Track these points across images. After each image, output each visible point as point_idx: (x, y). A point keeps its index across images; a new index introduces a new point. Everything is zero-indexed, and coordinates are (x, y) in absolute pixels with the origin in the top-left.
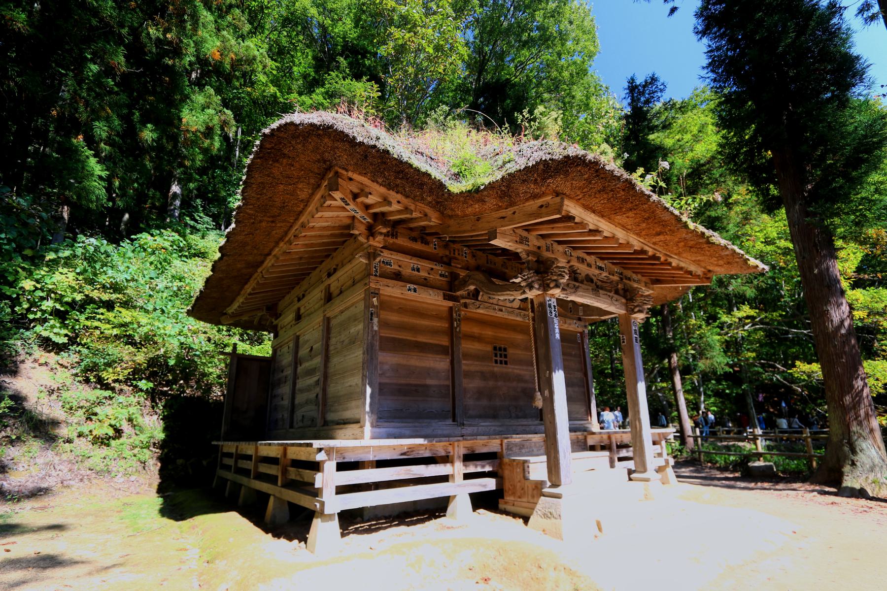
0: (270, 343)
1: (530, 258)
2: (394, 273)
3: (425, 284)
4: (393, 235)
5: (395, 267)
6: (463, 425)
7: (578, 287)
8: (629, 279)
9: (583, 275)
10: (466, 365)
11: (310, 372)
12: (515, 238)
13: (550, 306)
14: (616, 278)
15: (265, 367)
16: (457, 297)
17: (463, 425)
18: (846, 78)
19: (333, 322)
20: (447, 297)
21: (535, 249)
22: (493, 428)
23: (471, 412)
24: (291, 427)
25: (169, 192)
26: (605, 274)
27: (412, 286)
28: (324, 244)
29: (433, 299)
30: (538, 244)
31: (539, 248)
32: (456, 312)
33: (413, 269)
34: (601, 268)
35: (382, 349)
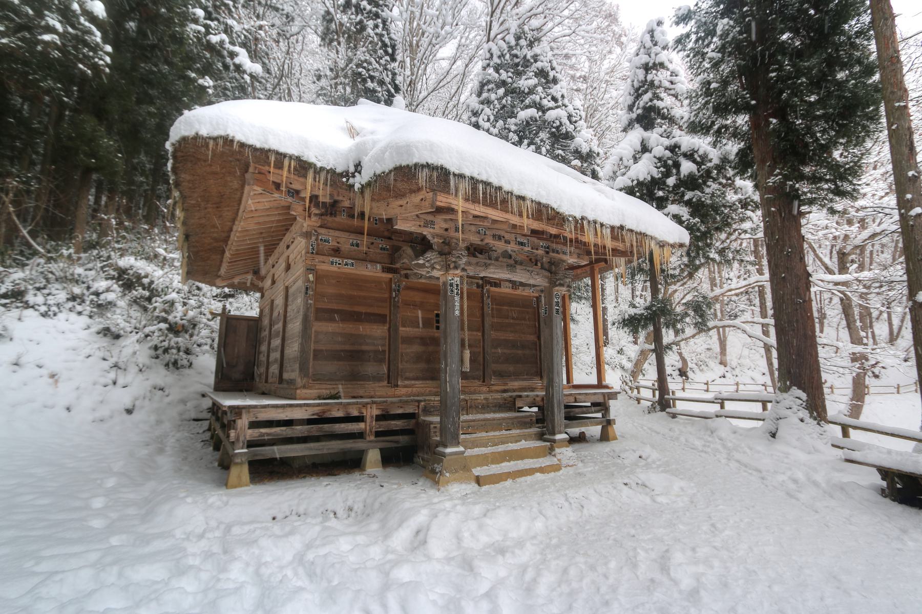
0: (257, 304)
1: (436, 240)
2: (333, 250)
3: (365, 259)
4: (331, 214)
5: (333, 244)
6: (397, 386)
7: (490, 265)
8: (558, 252)
9: (500, 251)
10: (404, 331)
11: (277, 335)
12: (418, 223)
13: (451, 285)
14: (540, 252)
15: (253, 324)
16: (397, 269)
17: (397, 386)
18: (790, 30)
19: (291, 291)
20: (386, 270)
21: (442, 232)
22: (429, 389)
23: (407, 374)
24: (266, 381)
25: (166, 136)
26: (526, 249)
27: (350, 261)
28: (278, 221)
29: (373, 271)
30: (445, 226)
31: (446, 230)
32: (395, 283)
33: (352, 245)
34: (522, 244)
35: (317, 319)
